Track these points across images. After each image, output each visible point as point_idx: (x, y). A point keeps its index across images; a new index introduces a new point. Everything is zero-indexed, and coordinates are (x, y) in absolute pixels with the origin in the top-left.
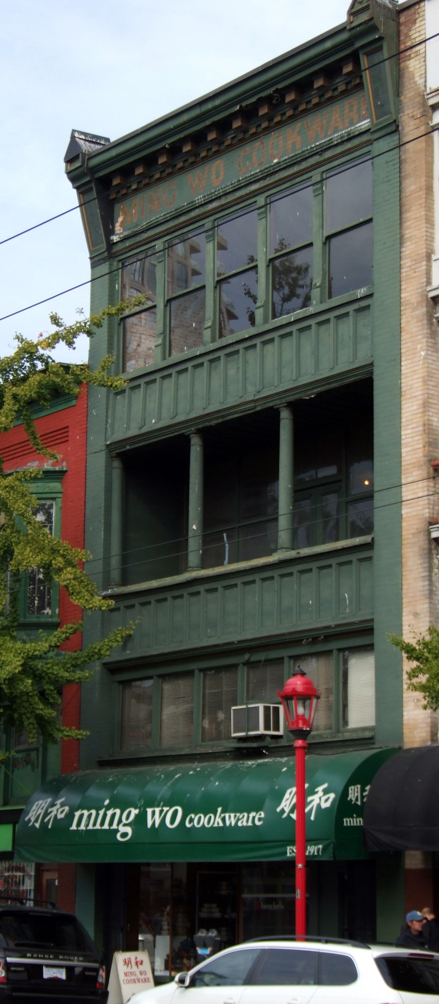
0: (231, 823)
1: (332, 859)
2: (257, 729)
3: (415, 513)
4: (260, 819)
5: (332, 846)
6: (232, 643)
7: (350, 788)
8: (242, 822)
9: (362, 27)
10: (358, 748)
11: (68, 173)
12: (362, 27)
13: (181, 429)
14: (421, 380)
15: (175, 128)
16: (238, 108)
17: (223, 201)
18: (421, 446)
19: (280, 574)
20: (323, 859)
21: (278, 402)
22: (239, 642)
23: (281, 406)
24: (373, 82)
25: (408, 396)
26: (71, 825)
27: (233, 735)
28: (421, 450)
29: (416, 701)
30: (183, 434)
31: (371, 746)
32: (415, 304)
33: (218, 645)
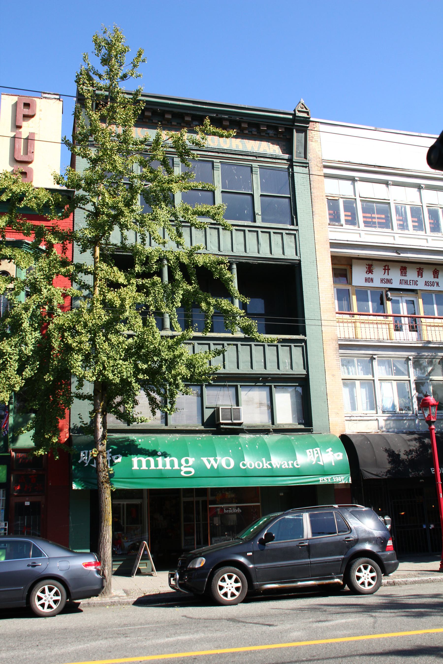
8: (285, 466)
21: (234, 260)
27: (221, 421)
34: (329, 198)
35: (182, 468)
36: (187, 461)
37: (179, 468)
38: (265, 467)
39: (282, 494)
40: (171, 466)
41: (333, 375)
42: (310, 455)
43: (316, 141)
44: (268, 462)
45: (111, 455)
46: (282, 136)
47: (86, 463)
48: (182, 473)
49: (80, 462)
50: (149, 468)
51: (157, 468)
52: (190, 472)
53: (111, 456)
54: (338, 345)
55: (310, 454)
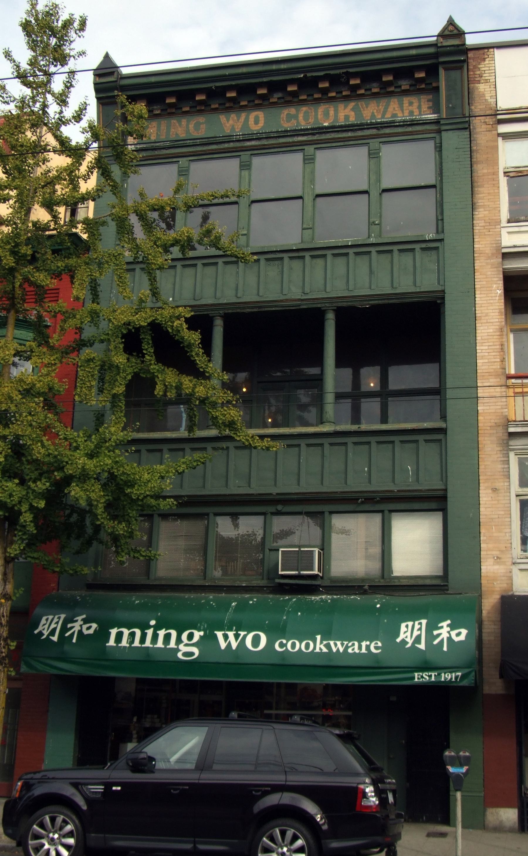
0: (338, 649)
1: (473, 685)
2: (312, 569)
3: (493, 411)
4: (376, 648)
5: (473, 673)
6: (271, 494)
7: (403, 625)
8: (353, 649)
9: (452, 48)
10: (434, 593)
11: (95, 84)
12: (452, 48)
13: (207, 310)
14: (498, 311)
15: (230, 75)
16: (302, 76)
17: (264, 142)
18: (499, 360)
19: (377, 441)
20: (461, 684)
21: (327, 305)
22: (277, 494)
23: (330, 308)
24: (448, 88)
25: (482, 321)
26: (108, 640)
27: (280, 573)
28: (498, 364)
29: (495, 558)
30: (208, 314)
31: (446, 592)
32: (490, 255)
33: (252, 495)
34: (511, 175)
35: (181, 647)
36: (190, 637)
37: (176, 647)
38: (317, 650)
39: (393, 699)
40: (151, 643)
41: (495, 490)
42: (405, 632)
43: (487, 81)
44: (325, 642)
45: (449, 629)
46: (423, 86)
47: (407, 643)
48: (180, 655)
49: (398, 640)
50: (117, 645)
51: (143, 646)
52: (192, 654)
53: (449, 632)
54: (507, 434)
55: (406, 629)
